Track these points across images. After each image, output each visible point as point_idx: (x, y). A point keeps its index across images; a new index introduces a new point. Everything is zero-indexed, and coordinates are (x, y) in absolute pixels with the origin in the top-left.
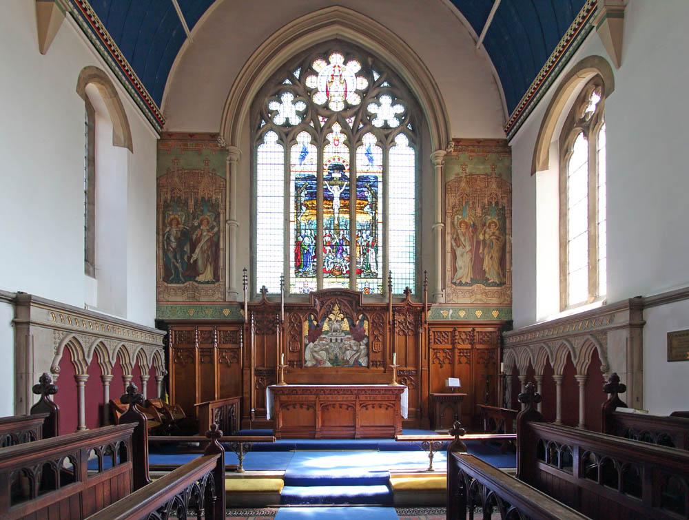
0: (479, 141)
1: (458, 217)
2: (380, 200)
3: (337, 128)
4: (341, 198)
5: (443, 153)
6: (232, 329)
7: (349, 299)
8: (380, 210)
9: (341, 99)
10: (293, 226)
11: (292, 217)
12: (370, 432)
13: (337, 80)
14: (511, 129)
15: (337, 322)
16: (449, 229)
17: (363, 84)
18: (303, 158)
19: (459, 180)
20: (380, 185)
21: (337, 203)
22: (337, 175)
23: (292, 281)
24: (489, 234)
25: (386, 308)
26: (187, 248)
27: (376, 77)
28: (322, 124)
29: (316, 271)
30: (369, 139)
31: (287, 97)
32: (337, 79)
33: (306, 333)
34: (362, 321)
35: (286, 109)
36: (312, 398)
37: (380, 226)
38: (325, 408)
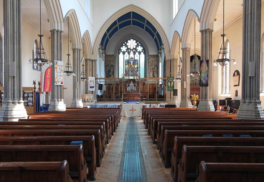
0: (154, 55)
2: (139, 63)
3: (132, 51)
4: (132, 63)
7: (134, 81)
8: (139, 65)
9: (132, 47)
10: (125, 68)
11: (125, 66)
12: (136, 100)
13: (132, 43)
15: (132, 84)
17: (136, 44)
18: (126, 57)
19: (151, 61)
22: (132, 59)
24: (155, 70)
26: (109, 73)
27: (138, 43)
28: (129, 51)
30: (137, 53)
31: (124, 47)
32: (132, 44)
33: (127, 86)
35: (124, 49)
36: (129, 95)
37: (139, 68)
38: (130, 97)
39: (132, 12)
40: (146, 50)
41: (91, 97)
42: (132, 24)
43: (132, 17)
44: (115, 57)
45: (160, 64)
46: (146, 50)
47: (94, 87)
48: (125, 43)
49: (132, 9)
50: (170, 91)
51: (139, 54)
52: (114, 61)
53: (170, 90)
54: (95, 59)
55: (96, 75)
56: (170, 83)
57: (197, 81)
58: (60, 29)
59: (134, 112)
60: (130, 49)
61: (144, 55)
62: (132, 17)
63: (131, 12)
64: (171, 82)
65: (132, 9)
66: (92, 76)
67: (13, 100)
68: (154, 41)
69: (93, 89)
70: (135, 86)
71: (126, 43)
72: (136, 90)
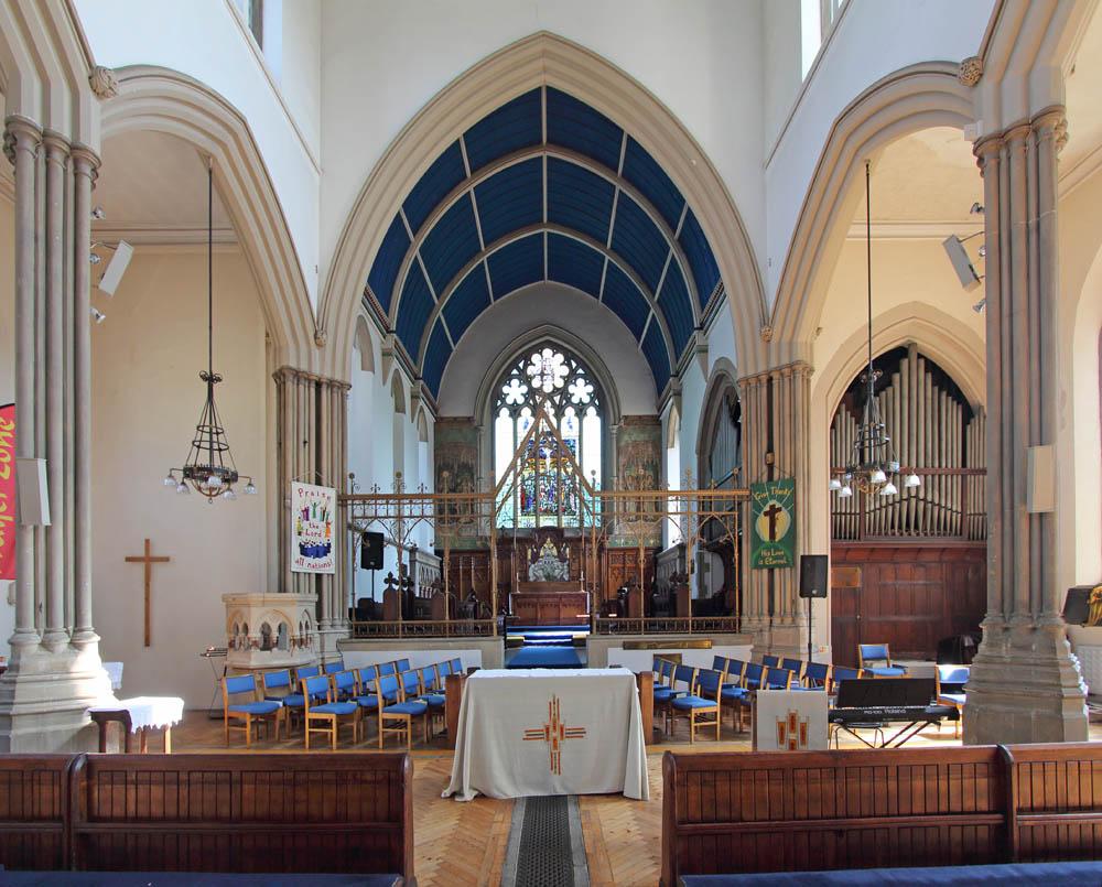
0: (640, 417)
1: (627, 473)
4: (551, 456)
5: (616, 427)
6: (481, 555)
7: (556, 534)
13: (550, 366)
14: (660, 408)
15: (549, 549)
16: (621, 481)
17: (565, 371)
20: (577, 446)
21: (548, 461)
23: (519, 518)
25: (580, 539)
27: (574, 365)
28: (538, 401)
29: (535, 511)
30: (570, 412)
31: (515, 382)
33: (529, 557)
34: (565, 549)
36: (535, 600)
38: (542, 607)
39: (549, 89)
40: (609, 392)
41: (287, 610)
42: (546, 216)
43: (545, 220)
44: (477, 429)
45: (673, 458)
46: (609, 392)
47: (326, 550)
48: (521, 365)
49: (545, 70)
50: (771, 571)
51: (577, 414)
52: (474, 449)
53: (770, 561)
54: (338, 377)
55: (344, 477)
56: (768, 518)
57: (921, 504)
58: (62, 127)
59: (567, 746)
60: (539, 390)
61: (598, 421)
62: (545, 220)
63: (540, 88)
64: (772, 513)
65: (545, 70)
66: (319, 482)
67: (46, 632)
68: (641, 352)
69: (324, 560)
70: (561, 557)
71: (526, 366)
72: (566, 577)
